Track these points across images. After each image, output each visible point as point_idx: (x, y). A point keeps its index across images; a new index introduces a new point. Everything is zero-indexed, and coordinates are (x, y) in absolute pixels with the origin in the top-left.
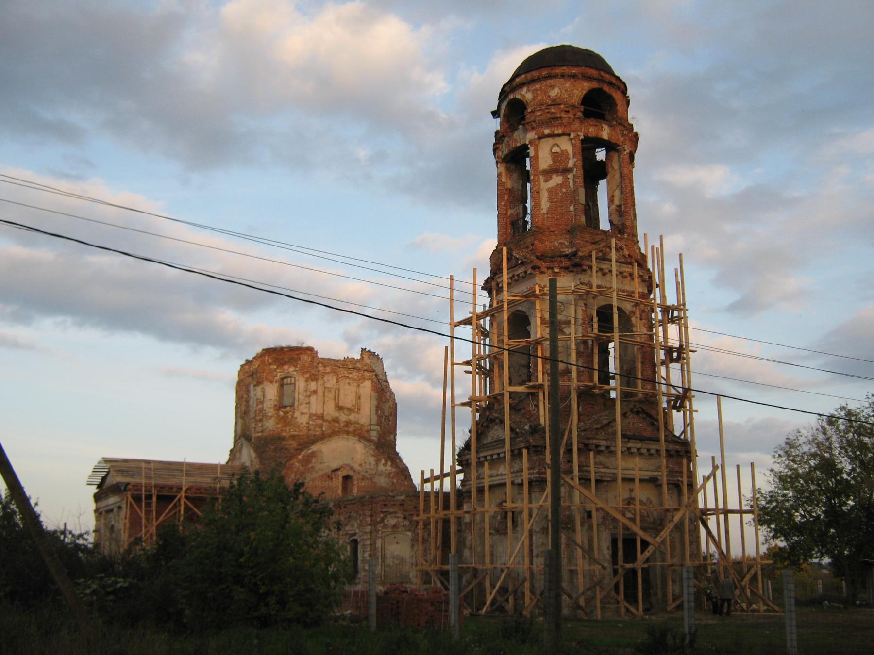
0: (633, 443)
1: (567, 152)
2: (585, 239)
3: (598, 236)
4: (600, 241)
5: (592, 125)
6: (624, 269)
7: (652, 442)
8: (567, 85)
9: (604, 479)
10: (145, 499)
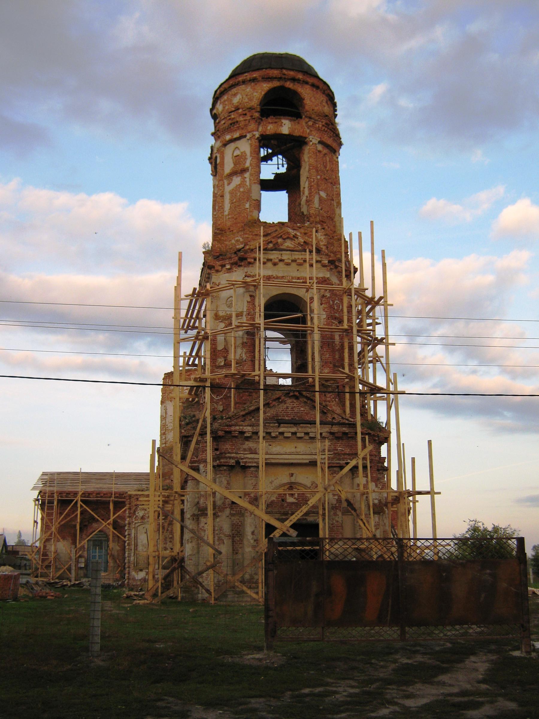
0: (284, 427)
1: (245, 153)
2: (254, 233)
3: (271, 228)
4: (272, 233)
5: (272, 123)
6: (297, 257)
7: (309, 426)
8: (248, 90)
9: (247, 465)
10: (48, 503)
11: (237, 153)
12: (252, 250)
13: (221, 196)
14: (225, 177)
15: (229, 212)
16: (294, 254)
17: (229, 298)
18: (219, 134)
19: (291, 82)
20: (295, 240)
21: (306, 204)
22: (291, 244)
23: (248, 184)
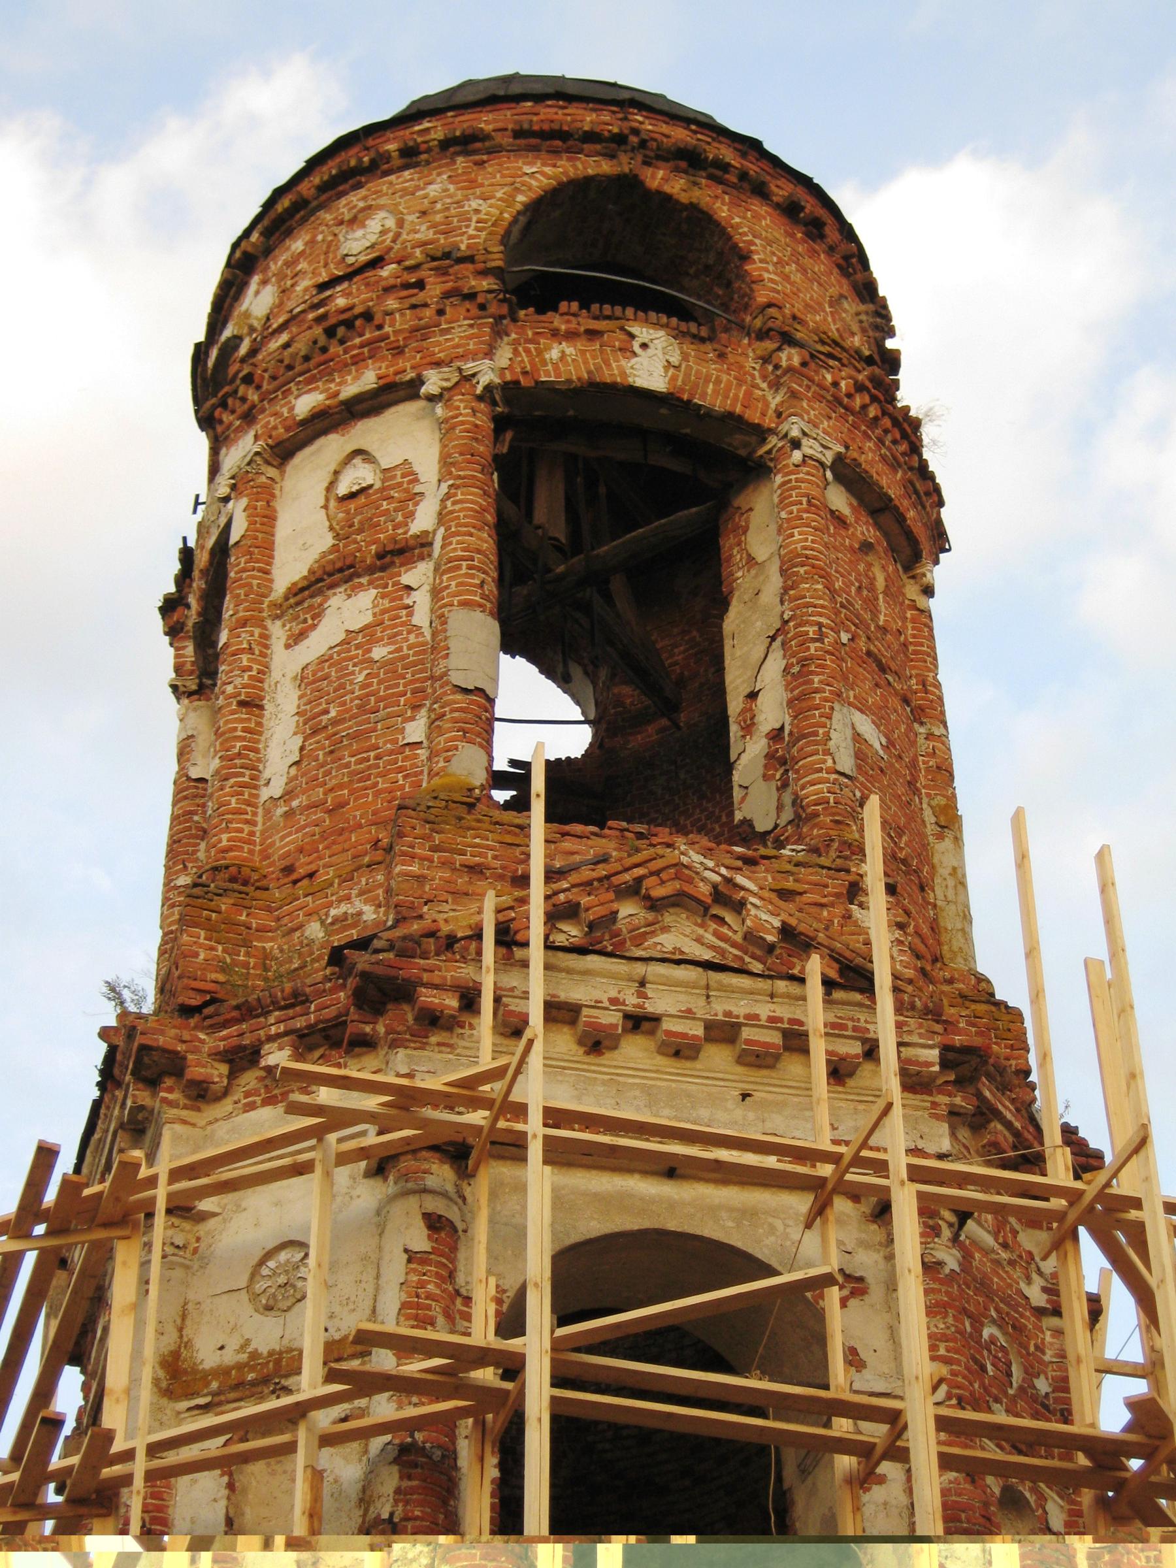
2: (469, 859)
6: (740, 1008)
8: (433, 190)
11: (360, 475)
12: (451, 942)
13: (242, 704)
14: (274, 605)
15: (291, 780)
16: (722, 988)
17: (262, 1262)
18: (253, 396)
19: (677, 170)
20: (721, 921)
21: (766, 777)
22: (699, 940)
23: (422, 617)
